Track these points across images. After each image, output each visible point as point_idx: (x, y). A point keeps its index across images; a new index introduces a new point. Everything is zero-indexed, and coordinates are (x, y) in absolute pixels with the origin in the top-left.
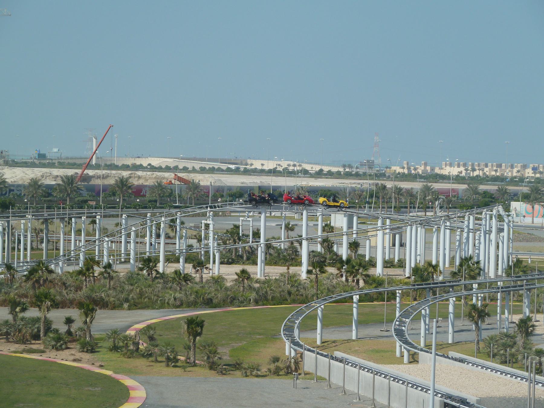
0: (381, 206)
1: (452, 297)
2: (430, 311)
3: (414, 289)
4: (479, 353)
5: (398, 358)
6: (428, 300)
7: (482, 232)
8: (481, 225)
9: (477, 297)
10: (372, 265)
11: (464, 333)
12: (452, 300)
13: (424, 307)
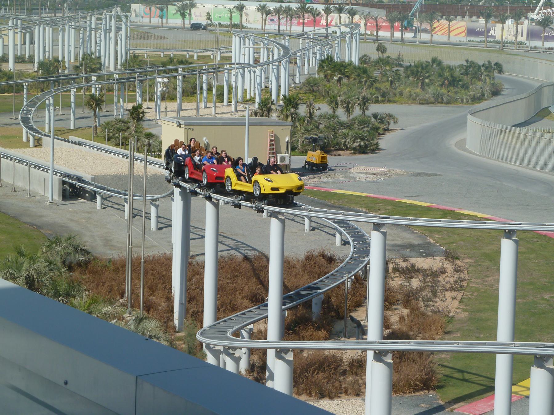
0: (14, 8)
1: (73, 88)
2: (54, 101)
3: (39, 81)
4: (96, 137)
5: (25, 142)
6: (51, 91)
7: (103, 31)
8: (101, 24)
9: (96, 88)
10: (5, 61)
11: (84, 120)
12: (73, 91)
13: (47, 97)
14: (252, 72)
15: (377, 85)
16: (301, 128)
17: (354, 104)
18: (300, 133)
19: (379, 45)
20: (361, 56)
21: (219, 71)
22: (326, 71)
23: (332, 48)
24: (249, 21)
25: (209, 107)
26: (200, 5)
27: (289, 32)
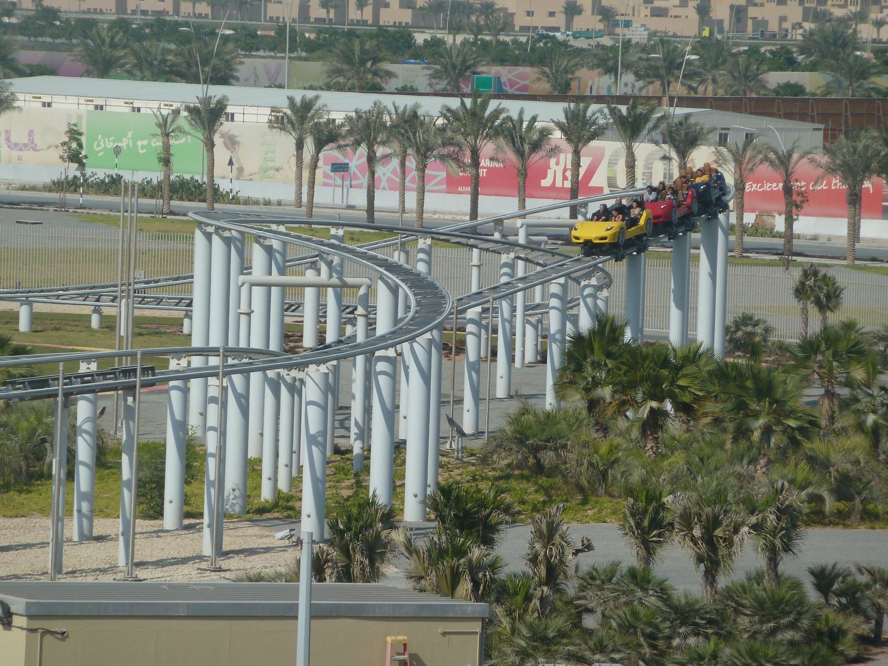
14: (284, 392)
15: (816, 446)
16: (514, 630)
17: (736, 531)
18: (509, 650)
19: (806, 274)
20: (730, 320)
21: (151, 384)
22: (596, 383)
23: (608, 286)
24: (241, 170)
25: (100, 539)
26: (29, 97)
27: (411, 217)
